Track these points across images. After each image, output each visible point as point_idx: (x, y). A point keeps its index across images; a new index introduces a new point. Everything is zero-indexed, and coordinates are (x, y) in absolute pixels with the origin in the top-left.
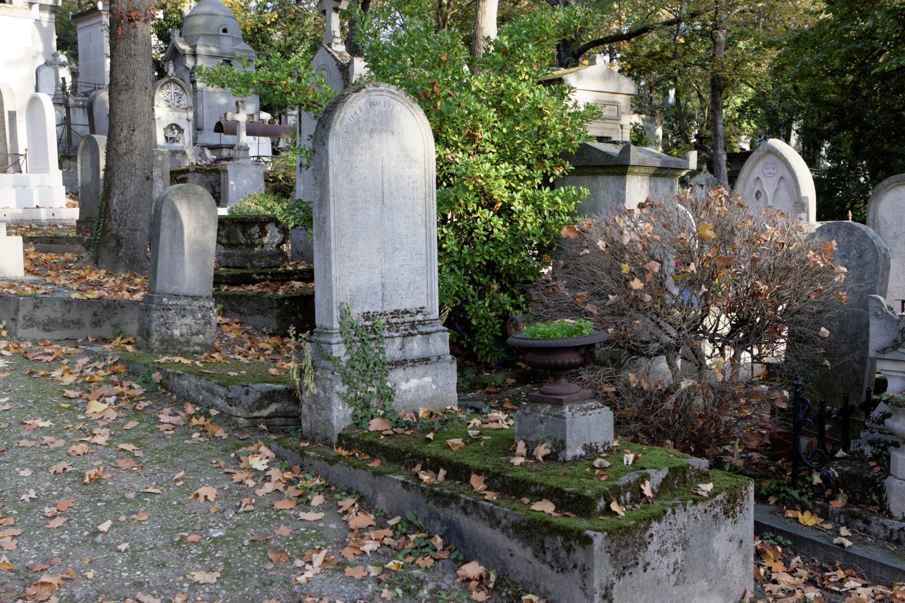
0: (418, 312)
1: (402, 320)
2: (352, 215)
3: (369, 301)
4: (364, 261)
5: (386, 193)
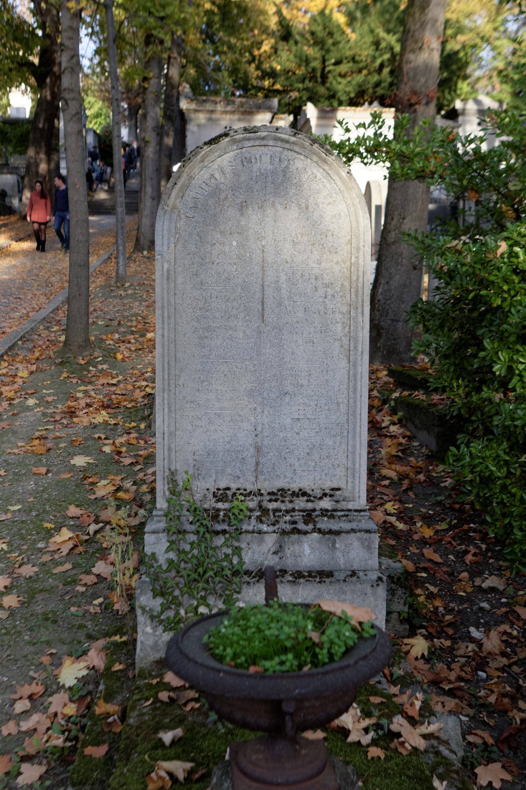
0: (325, 495)
1: (290, 506)
3: (229, 470)
4: (221, 409)
5: (270, 302)
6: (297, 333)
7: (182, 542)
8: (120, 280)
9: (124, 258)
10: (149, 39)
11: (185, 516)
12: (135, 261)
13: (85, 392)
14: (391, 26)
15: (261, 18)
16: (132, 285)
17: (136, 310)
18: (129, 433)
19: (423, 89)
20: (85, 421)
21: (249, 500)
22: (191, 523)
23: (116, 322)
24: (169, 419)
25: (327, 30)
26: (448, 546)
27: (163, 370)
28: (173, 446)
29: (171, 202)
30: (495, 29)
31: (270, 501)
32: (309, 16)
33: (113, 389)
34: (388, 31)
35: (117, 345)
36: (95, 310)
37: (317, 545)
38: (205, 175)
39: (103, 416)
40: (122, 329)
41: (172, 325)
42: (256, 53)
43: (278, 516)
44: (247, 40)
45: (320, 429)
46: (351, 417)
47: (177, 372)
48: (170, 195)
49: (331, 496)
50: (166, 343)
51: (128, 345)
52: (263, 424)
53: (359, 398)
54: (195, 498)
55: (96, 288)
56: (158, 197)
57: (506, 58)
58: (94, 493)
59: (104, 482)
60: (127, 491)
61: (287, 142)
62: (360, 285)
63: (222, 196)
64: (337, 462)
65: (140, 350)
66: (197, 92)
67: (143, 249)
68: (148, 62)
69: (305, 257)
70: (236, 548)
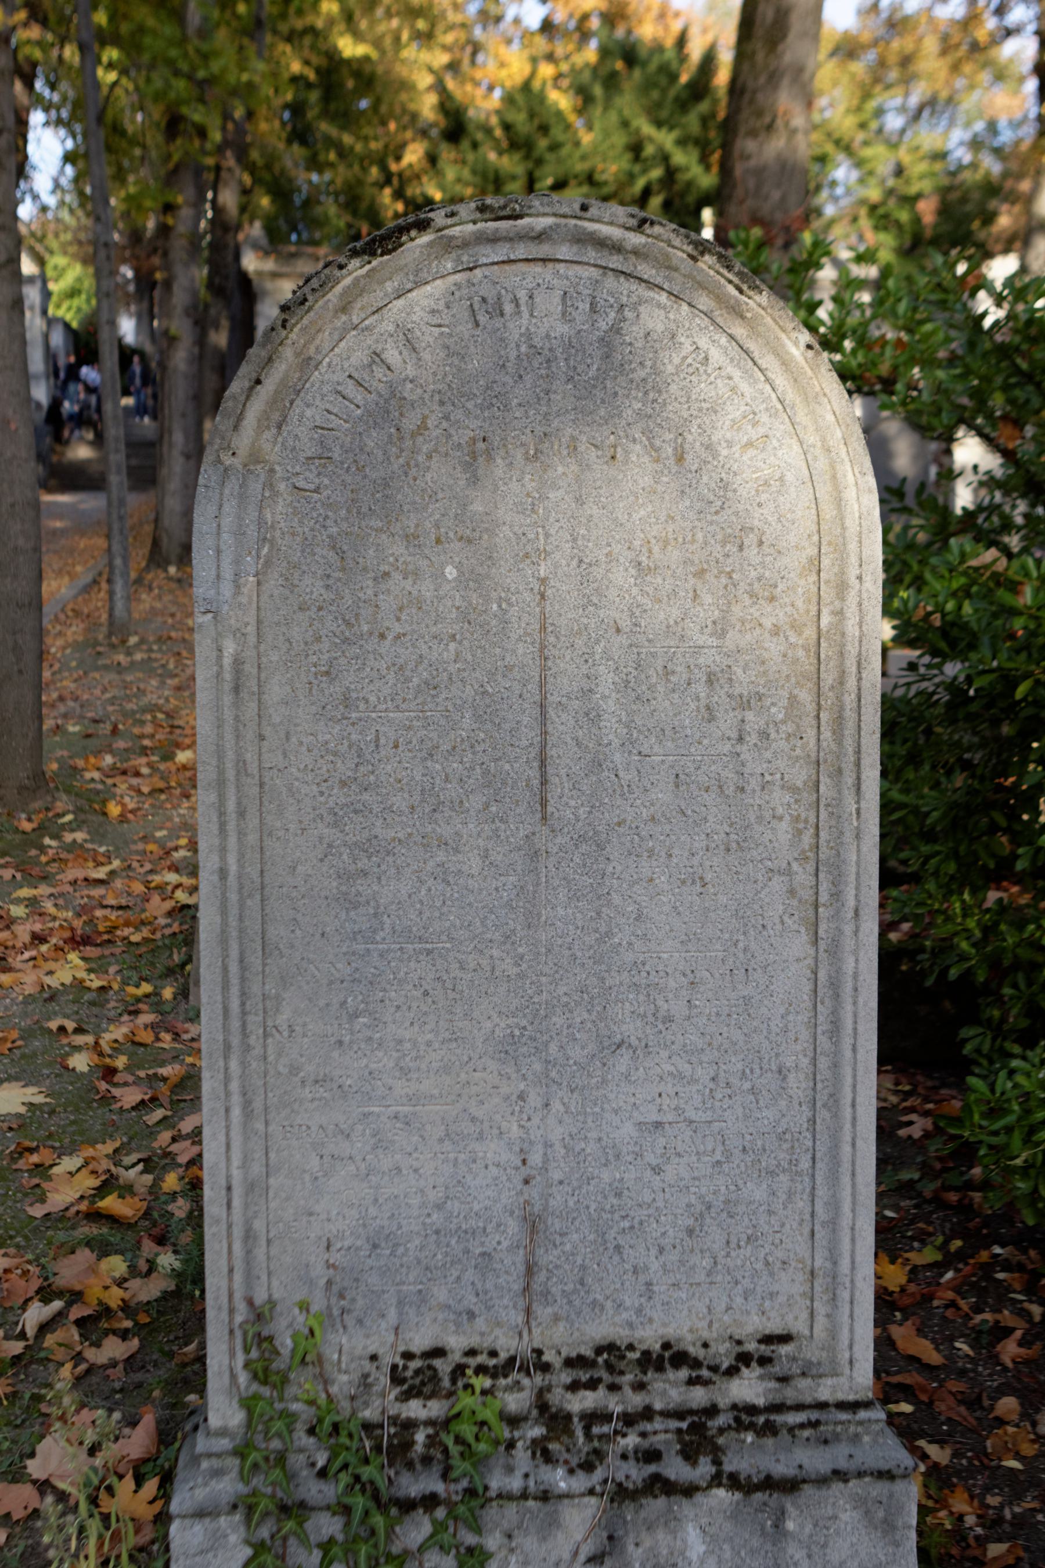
0: (745, 1359)
1: (636, 1401)
2: (345, 876)
3: (440, 1294)
4: (412, 1099)
5: (564, 759)
6: (651, 852)
7: (292, 1541)
8: (118, 631)
9: (126, 583)
10: (174, 125)
11: (301, 1450)
12: (151, 589)
13: (32, 903)
14: (664, 114)
15: (404, 96)
16: (142, 641)
17: (151, 698)
18: (136, 1013)
19: (779, 216)
20: (29, 980)
21: (508, 1389)
22: (323, 1474)
23: (108, 727)
24: (246, 1139)
25: (536, 122)
26: (950, 1313)
27: (226, 986)
28: (259, 1225)
29: (244, 440)
30: (863, 126)
31: (574, 1387)
32: (497, 93)
33: (97, 892)
34: (659, 124)
35: (109, 781)
36: (61, 699)
37: (728, 1526)
38: (352, 352)
39: (70, 969)
40: (121, 744)
41: (252, 838)
42: (394, 167)
43: (601, 1437)
44: (376, 138)
45: (728, 1155)
46: (823, 1114)
47: (271, 988)
48: (240, 418)
49: (764, 1361)
50: (233, 897)
51: (134, 781)
52: (548, 1145)
53: (848, 1054)
54: (334, 1390)
55: (64, 648)
56: (196, 453)
57: (883, 181)
58: (43, 1200)
59: (70, 1163)
60: (127, 1190)
61: (617, 248)
62: (850, 700)
63: (410, 423)
64: (780, 1254)
65: (161, 791)
66: (275, 240)
67: (168, 562)
68: (176, 170)
69: (676, 613)
70: (471, 1550)
